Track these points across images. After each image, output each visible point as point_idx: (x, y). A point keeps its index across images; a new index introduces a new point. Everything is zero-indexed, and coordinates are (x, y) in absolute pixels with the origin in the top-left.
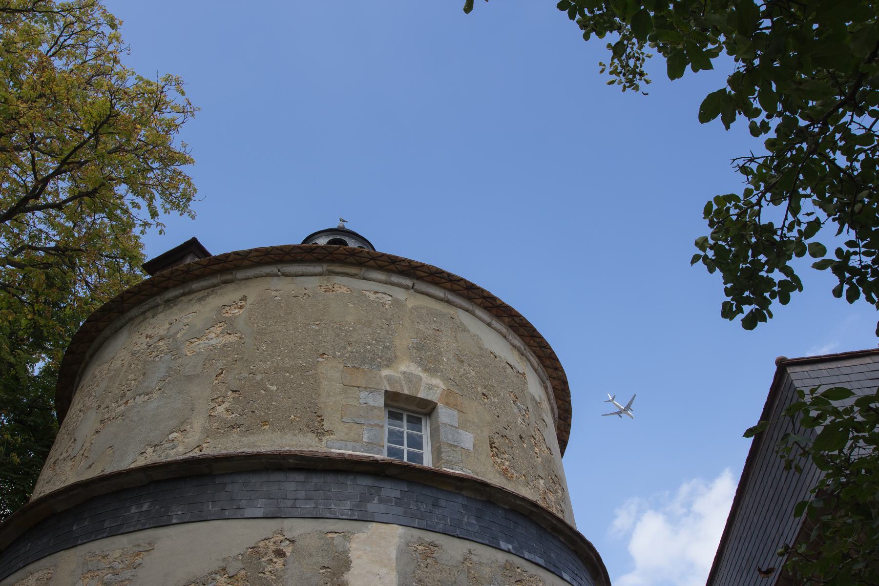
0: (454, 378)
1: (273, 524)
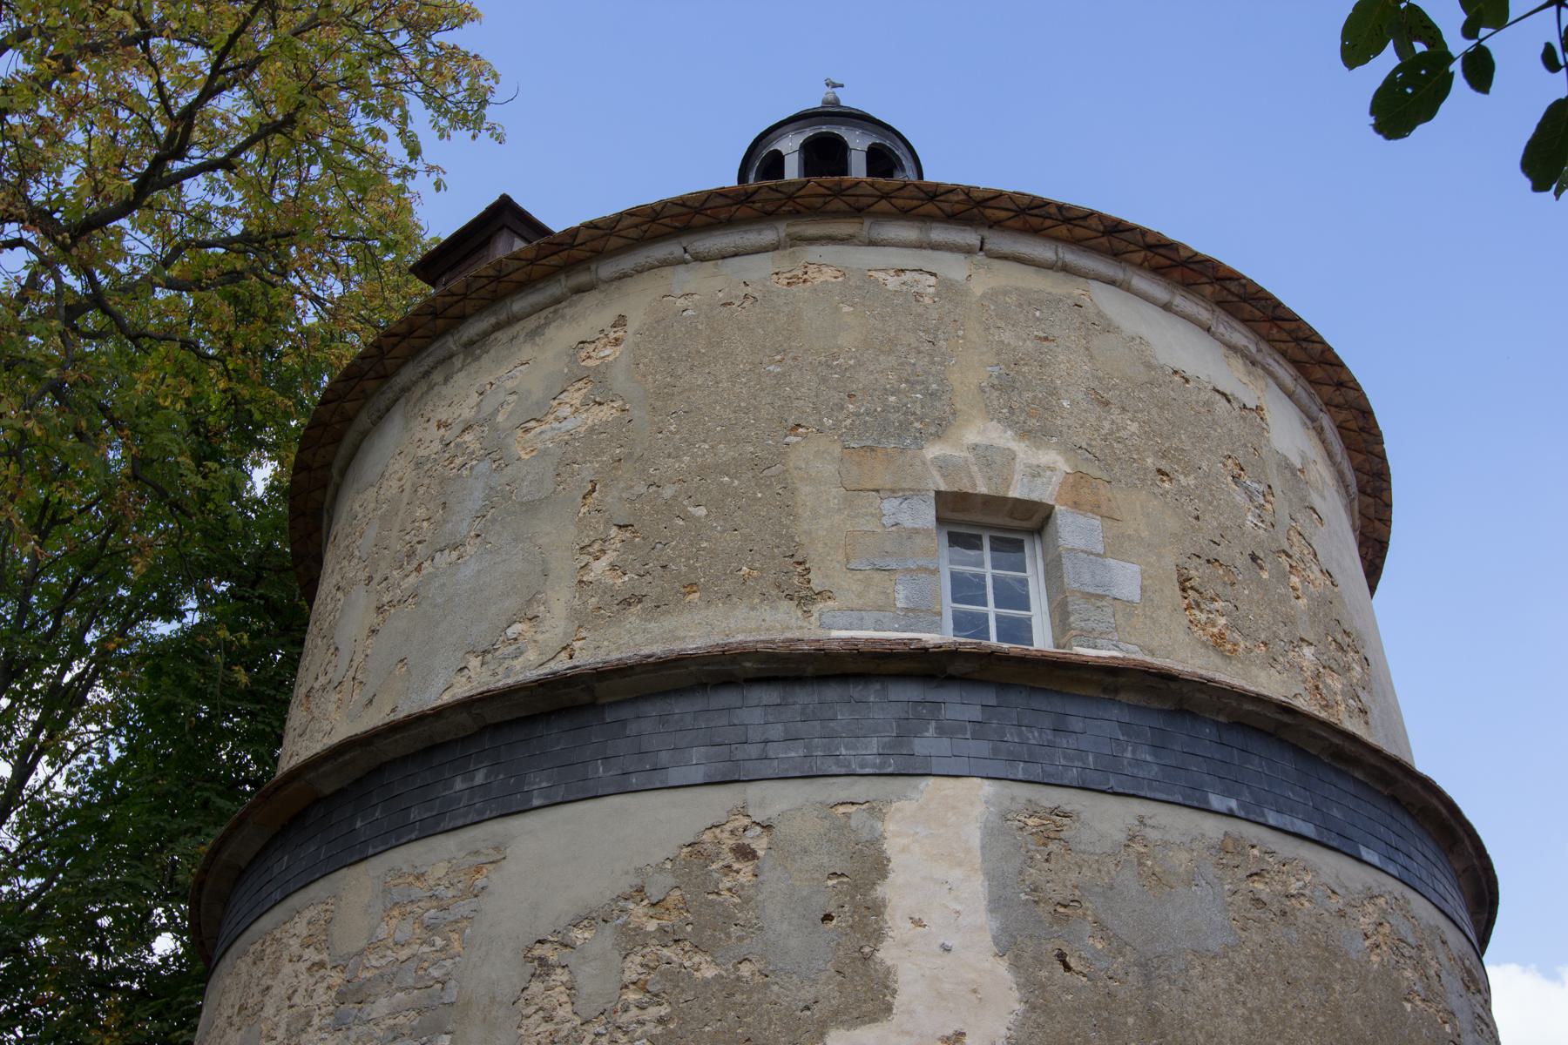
0: (1088, 444)
1: (722, 799)
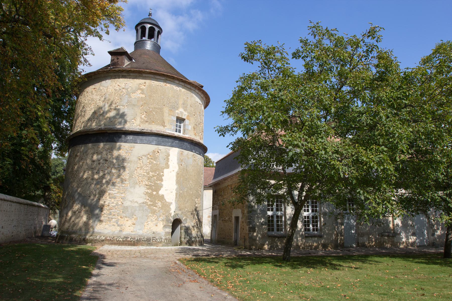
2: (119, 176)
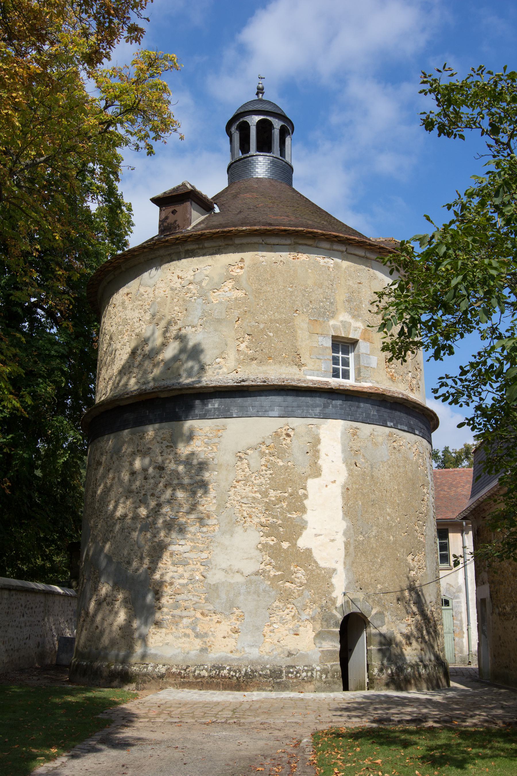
1: (283, 421)
2: (193, 508)
